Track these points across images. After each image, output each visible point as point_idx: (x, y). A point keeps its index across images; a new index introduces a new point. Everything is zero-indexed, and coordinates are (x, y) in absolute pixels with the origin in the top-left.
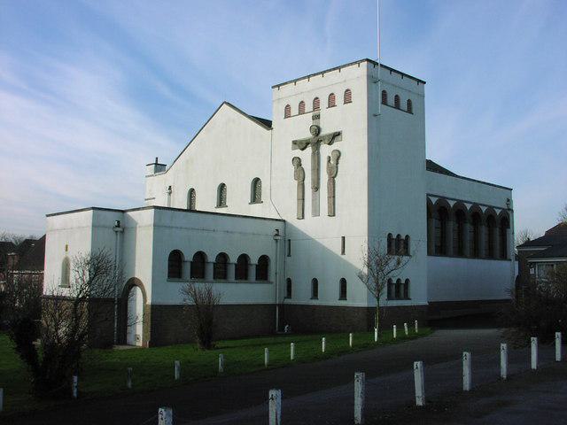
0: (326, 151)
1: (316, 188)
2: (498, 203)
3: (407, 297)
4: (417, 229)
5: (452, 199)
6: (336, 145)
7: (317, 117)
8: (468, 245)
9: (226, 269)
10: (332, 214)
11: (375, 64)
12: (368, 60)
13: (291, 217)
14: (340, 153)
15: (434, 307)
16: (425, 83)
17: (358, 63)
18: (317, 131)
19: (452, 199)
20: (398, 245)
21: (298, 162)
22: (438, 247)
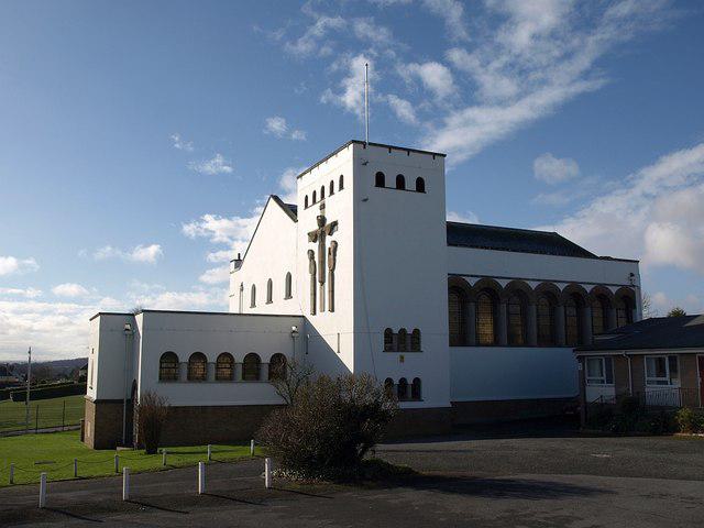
0: (329, 240)
1: (322, 283)
2: (614, 279)
3: (82, 364)
4: (434, 320)
5: (533, 280)
6: (334, 237)
7: (323, 207)
8: (504, 337)
9: (259, 369)
10: (332, 310)
11: (364, 143)
12: (353, 142)
13: (307, 313)
14: (336, 243)
15: (458, 407)
16: (445, 156)
17: (345, 146)
18: (322, 220)
19: (533, 280)
20: (402, 341)
21: (311, 253)
22: (461, 335)
